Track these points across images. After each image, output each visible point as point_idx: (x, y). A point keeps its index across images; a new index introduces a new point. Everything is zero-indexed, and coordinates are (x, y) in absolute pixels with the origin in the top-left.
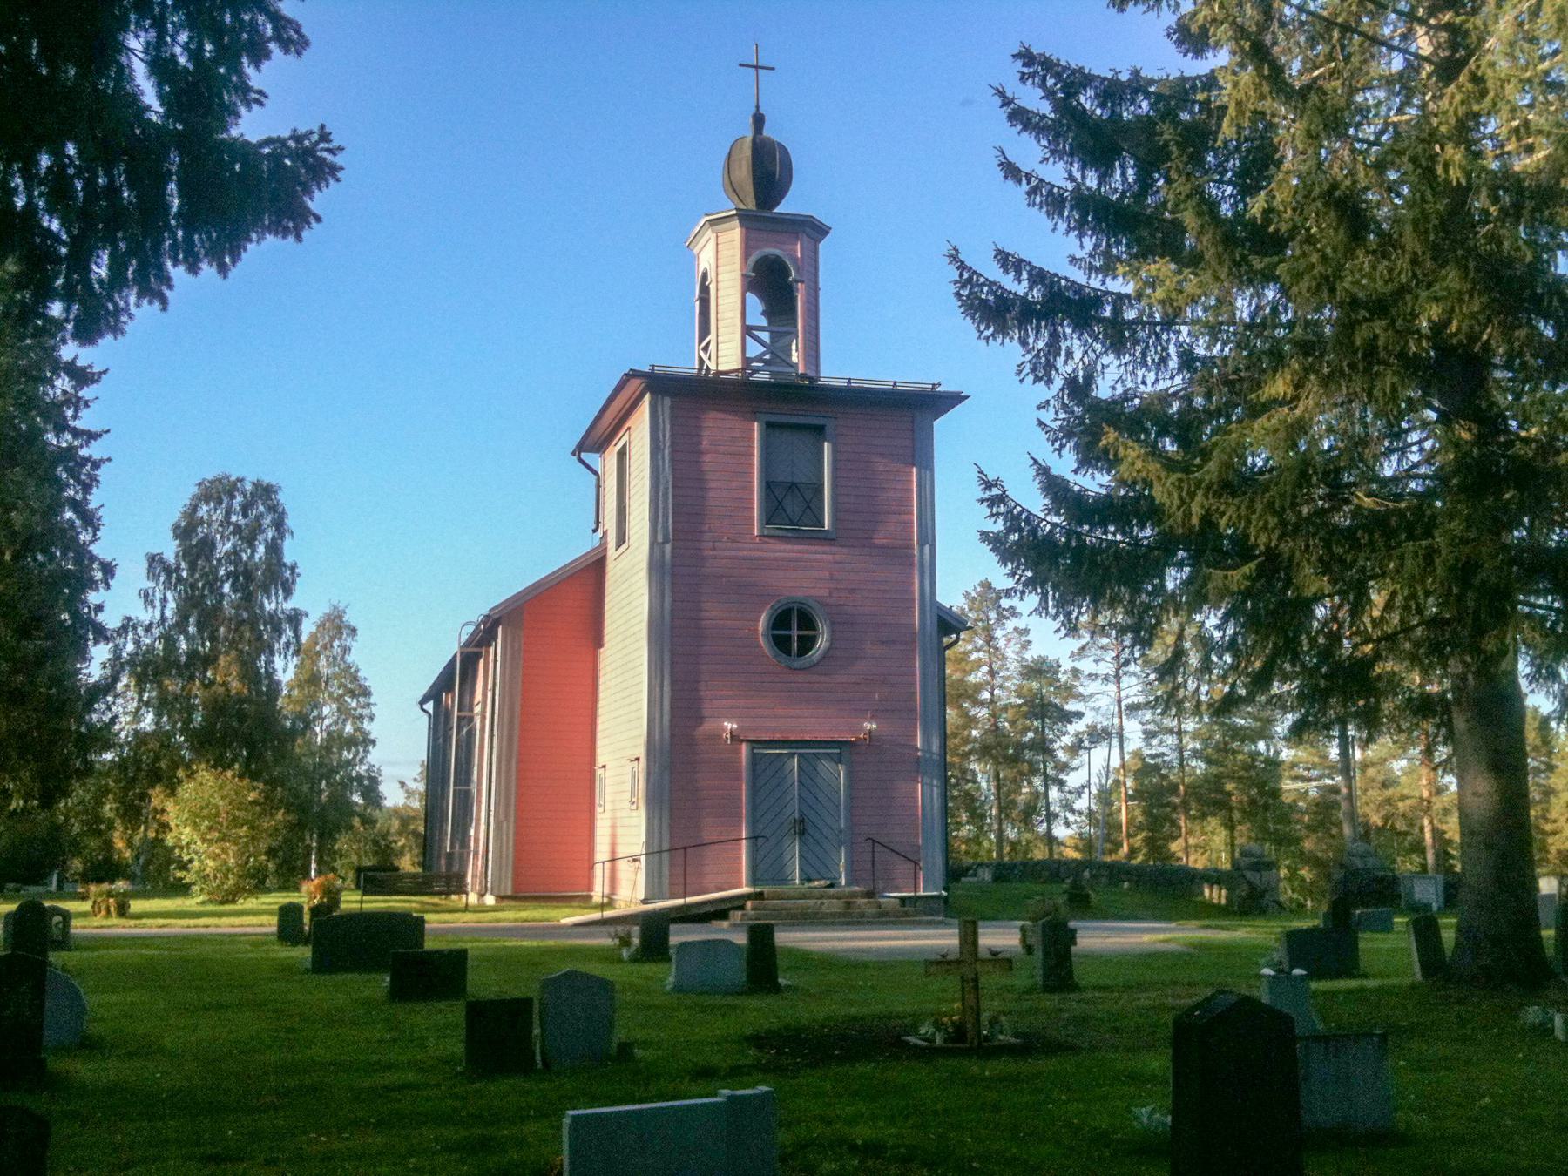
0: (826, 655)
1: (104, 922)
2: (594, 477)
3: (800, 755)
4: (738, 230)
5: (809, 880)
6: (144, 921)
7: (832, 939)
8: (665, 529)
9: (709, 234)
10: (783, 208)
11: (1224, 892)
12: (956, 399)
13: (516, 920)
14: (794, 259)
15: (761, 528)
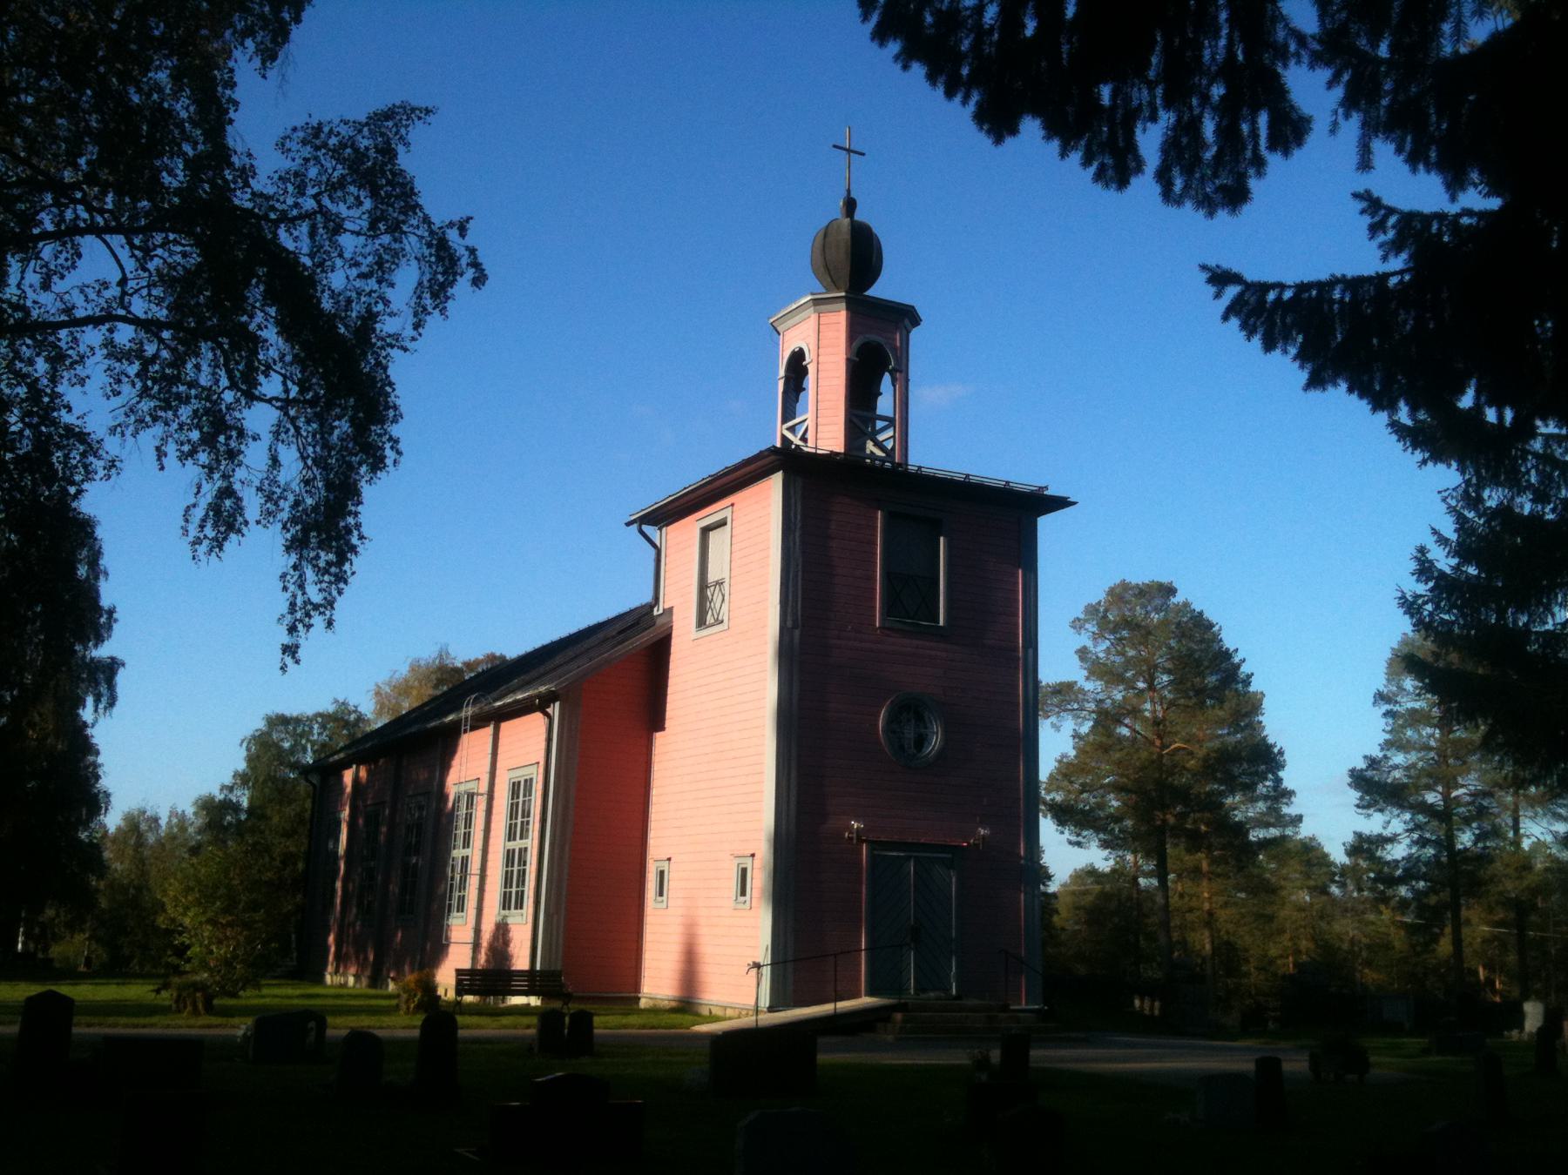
2: (653, 552)
4: (844, 313)
5: (924, 990)
7: (1096, 1060)
8: (795, 614)
9: (811, 313)
10: (871, 292)
11: (1157, 1004)
12: (1061, 503)
13: (644, 1027)
14: (894, 349)
15: (882, 620)
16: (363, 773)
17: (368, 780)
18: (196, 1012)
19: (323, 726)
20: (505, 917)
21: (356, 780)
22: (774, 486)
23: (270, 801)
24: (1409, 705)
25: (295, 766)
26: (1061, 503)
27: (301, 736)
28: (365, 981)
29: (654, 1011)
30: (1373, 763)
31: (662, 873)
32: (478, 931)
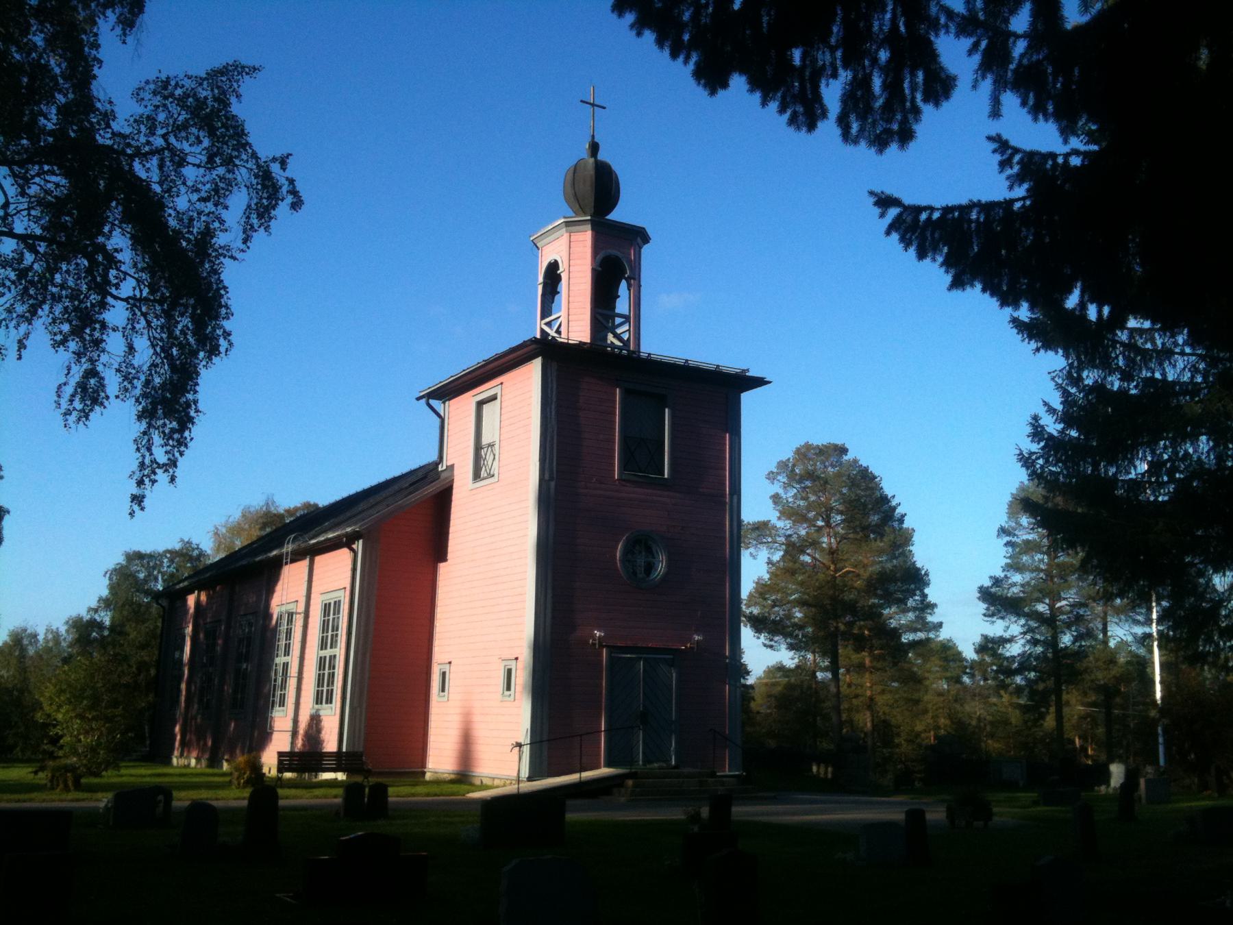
0: (665, 578)
1: (64, 796)
2: (438, 420)
3: (646, 660)
5: (650, 762)
6: (33, 795)
11: (830, 769)
12: (759, 382)
16: (203, 597)
19: (171, 561)
20: (318, 710)
21: (198, 603)
23: (128, 620)
24: (1025, 537)
25: (148, 592)
26: (759, 382)
27: (154, 568)
28: (204, 763)
29: (437, 782)
30: (997, 582)
32: (296, 721)
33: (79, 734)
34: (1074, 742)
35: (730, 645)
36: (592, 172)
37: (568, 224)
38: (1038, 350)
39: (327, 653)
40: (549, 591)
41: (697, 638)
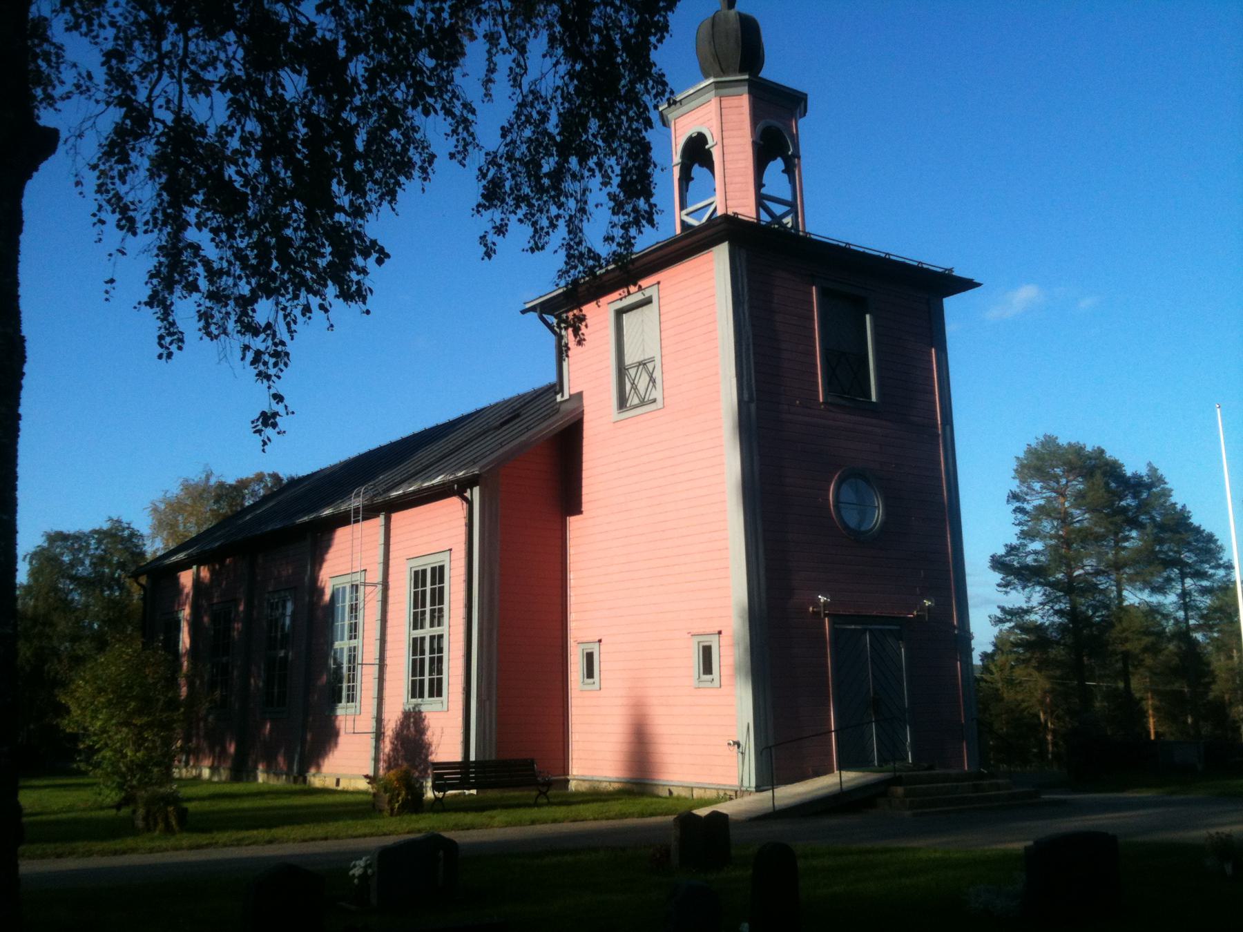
3: (871, 631)
12: (966, 285)
16: (205, 573)
17: (212, 579)
18: (169, 830)
19: (99, 542)
20: (416, 705)
21: (197, 582)
22: (718, 259)
23: (56, 609)
24: (1036, 503)
25: (74, 579)
26: (966, 285)
27: (79, 550)
28: (224, 774)
29: (595, 796)
30: (1012, 550)
31: (590, 657)
32: (379, 720)
33: (124, 745)
34: (1039, 718)
35: (958, 610)
36: (737, 26)
37: (718, 85)
38: (208, 478)
39: (427, 632)
40: (761, 546)
41: (927, 603)
